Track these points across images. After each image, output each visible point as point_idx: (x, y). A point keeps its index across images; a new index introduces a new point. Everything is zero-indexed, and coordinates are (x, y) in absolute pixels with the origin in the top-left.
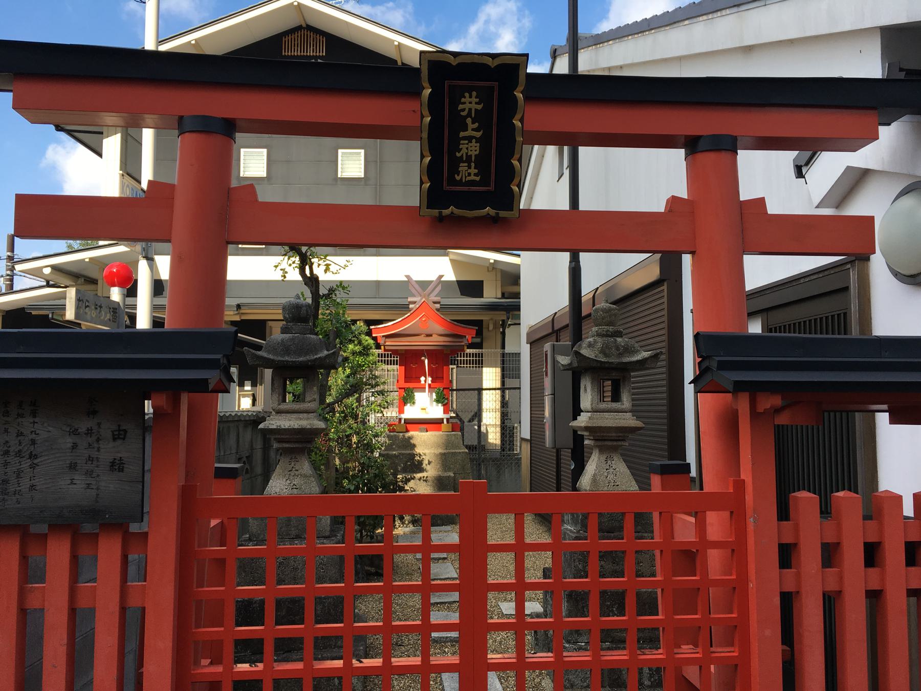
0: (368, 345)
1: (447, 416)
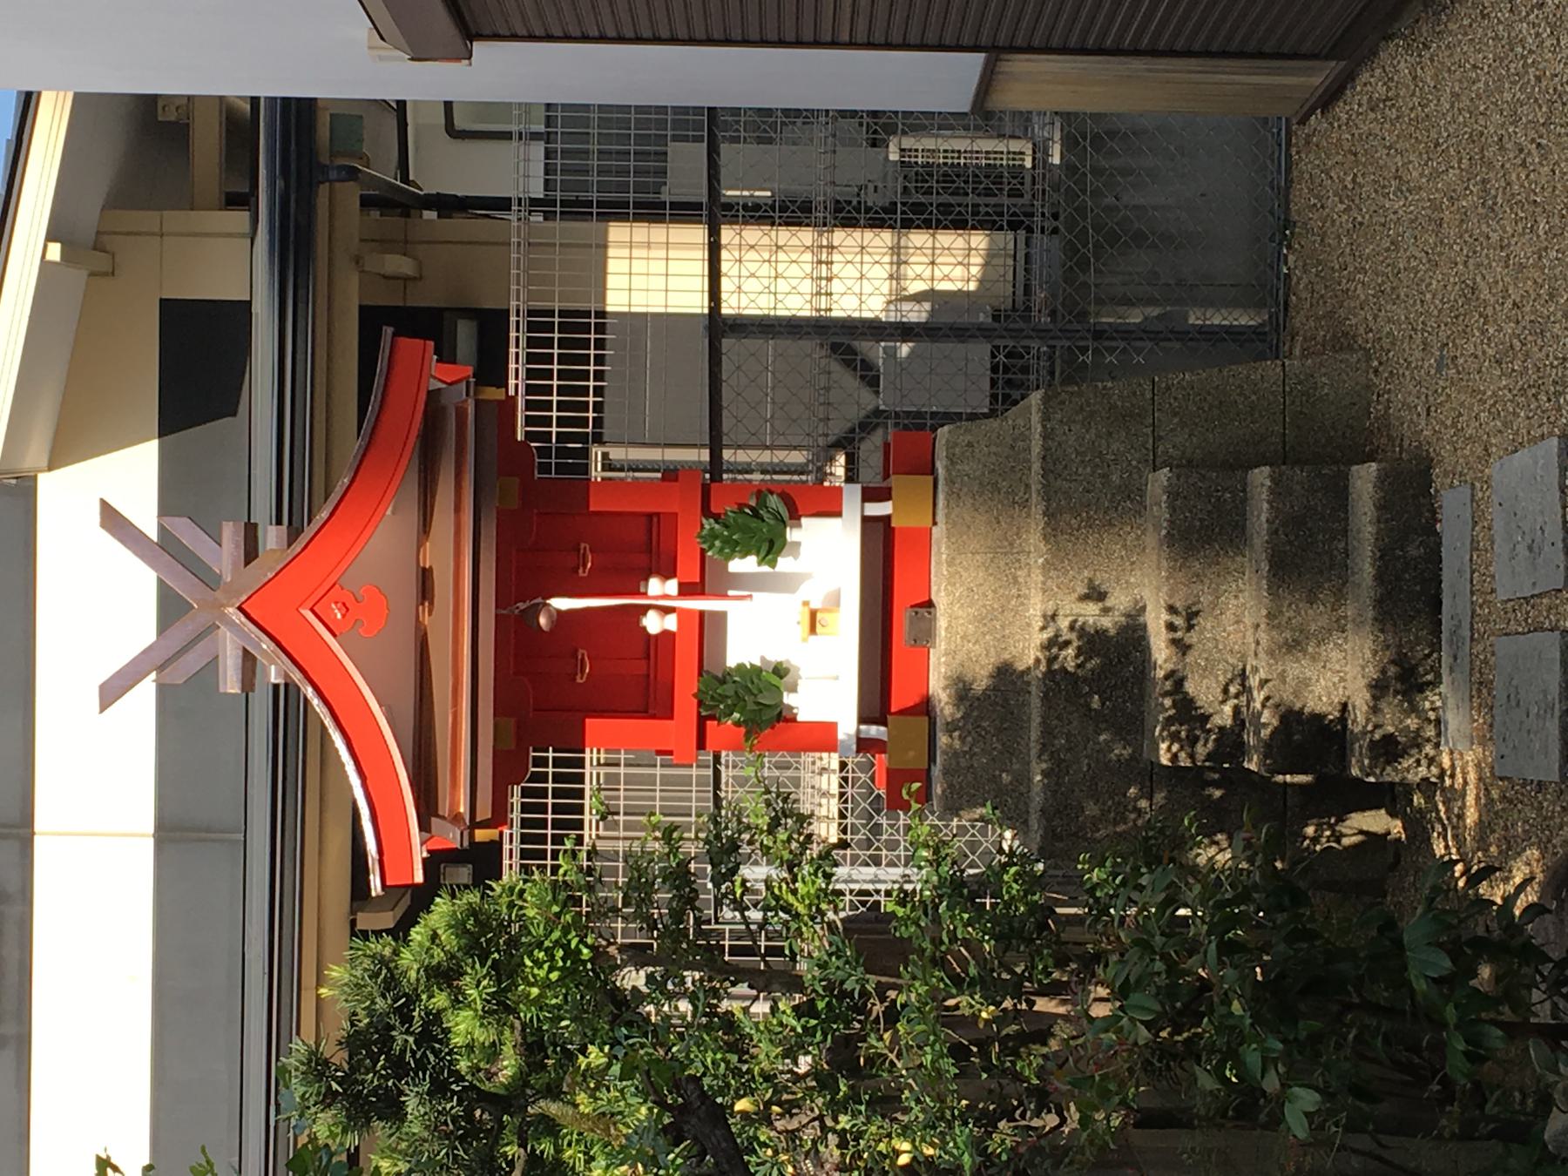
0: (458, 927)
1: (852, 495)
